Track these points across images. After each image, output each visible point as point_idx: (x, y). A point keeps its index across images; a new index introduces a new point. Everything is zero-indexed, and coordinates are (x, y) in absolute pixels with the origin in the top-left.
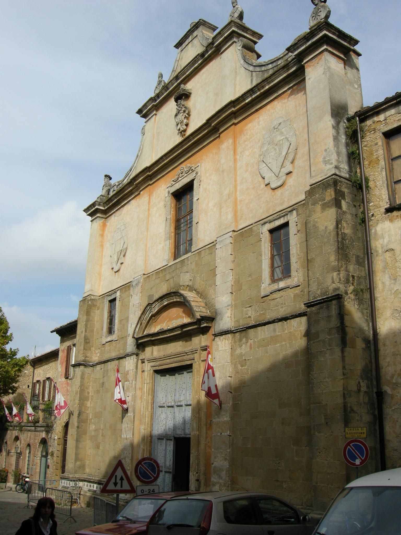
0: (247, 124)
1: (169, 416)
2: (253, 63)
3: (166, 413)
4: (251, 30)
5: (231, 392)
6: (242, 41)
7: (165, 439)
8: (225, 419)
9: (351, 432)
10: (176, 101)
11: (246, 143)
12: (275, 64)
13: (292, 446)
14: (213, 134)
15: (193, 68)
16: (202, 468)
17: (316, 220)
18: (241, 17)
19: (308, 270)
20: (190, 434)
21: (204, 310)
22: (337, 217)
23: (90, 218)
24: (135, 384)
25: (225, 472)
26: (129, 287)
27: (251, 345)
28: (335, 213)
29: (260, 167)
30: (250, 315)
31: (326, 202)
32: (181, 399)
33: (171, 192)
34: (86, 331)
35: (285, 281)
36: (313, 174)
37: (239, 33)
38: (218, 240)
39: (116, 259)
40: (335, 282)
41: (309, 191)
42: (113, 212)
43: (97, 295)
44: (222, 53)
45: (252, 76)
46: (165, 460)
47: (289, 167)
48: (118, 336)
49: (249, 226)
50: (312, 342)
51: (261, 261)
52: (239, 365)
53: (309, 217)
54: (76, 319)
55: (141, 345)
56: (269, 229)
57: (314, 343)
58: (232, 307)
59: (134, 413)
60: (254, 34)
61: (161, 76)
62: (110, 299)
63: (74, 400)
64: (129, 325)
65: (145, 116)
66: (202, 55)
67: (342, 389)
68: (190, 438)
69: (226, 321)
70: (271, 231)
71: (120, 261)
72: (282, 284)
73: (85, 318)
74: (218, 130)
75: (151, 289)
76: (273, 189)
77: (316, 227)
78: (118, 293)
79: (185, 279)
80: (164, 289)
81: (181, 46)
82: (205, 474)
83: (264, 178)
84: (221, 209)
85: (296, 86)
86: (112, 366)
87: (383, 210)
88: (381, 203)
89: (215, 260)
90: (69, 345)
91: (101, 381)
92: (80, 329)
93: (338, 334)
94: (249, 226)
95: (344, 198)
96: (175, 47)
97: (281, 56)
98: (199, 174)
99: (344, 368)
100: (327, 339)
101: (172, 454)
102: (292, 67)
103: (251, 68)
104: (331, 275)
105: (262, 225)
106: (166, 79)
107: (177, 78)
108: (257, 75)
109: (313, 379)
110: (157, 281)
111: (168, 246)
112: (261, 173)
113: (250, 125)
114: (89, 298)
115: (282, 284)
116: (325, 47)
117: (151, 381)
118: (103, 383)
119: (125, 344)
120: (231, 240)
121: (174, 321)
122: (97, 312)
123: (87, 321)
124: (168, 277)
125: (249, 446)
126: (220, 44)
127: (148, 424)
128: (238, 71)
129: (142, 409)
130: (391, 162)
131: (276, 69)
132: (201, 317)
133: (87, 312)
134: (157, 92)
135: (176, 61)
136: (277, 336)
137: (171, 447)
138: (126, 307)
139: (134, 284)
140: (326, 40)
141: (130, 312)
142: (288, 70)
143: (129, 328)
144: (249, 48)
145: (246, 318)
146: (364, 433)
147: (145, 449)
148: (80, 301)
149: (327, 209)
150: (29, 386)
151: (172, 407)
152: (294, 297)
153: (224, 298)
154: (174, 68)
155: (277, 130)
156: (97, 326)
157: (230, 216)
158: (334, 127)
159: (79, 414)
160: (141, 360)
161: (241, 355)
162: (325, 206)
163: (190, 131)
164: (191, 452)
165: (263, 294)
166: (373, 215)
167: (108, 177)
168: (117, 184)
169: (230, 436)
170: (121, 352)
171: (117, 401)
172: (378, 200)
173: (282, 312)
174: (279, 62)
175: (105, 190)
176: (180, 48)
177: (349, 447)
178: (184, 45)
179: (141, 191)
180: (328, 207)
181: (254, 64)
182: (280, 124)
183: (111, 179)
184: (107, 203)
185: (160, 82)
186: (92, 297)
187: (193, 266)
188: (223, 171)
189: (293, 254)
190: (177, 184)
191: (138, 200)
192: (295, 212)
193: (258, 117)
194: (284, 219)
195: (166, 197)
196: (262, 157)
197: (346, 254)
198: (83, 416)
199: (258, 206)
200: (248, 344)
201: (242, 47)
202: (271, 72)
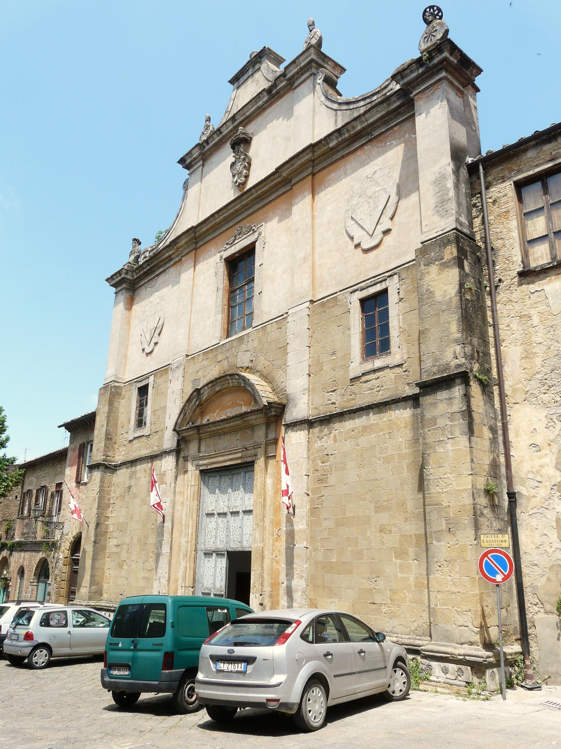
0: (329, 174)
1: (220, 525)
2: (338, 100)
3: (216, 522)
4: (333, 61)
5: (308, 495)
6: (322, 72)
7: (214, 554)
8: (300, 527)
9: (488, 539)
10: (233, 147)
11: (328, 196)
12: (368, 100)
13: (394, 559)
14: (282, 187)
15: (256, 107)
16: (267, 589)
17: (430, 283)
18: (319, 43)
19: (419, 343)
20: (251, 547)
21: (271, 395)
22: (460, 280)
23: (114, 290)
24: (175, 487)
25: (300, 593)
26: (167, 370)
27: (335, 436)
28: (458, 274)
29: (348, 225)
30: (333, 401)
31: (446, 261)
32: (237, 504)
33: (224, 257)
34: (107, 425)
35: (382, 359)
36: (424, 229)
37: (316, 65)
38: (290, 312)
39: (148, 338)
40: (458, 358)
41: (421, 249)
42: (143, 282)
43: (121, 381)
44: (295, 88)
45: (336, 115)
46: (215, 581)
47: (386, 224)
48: (151, 430)
49: (332, 294)
50: (426, 430)
51: (349, 336)
52: (319, 462)
53: (421, 279)
54: (94, 411)
55: (182, 442)
56: (360, 297)
57: (429, 431)
58: (309, 392)
59: (173, 522)
60: (336, 65)
61: (209, 119)
62: (140, 386)
63: (91, 509)
64: (167, 416)
65: (188, 167)
66: (269, 91)
67: (471, 487)
68: (250, 552)
69: (300, 409)
70: (363, 301)
71: (154, 341)
72: (378, 363)
73: (106, 409)
74: (291, 181)
75: (197, 372)
76: (366, 251)
77: (431, 293)
78: (152, 379)
79: (243, 360)
80: (214, 372)
81: (237, 81)
82: (271, 596)
83: (353, 238)
84: (293, 275)
85: (398, 126)
86: (140, 468)
87: (515, 273)
88: (510, 265)
89: (287, 336)
90: (81, 442)
91: (127, 485)
92: (100, 422)
93: (464, 420)
94: (332, 294)
95: (467, 259)
96: (229, 82)
97: (377, 90)
98: (263, 235)
99: (472, 461)
100: (448, 426)
101: (224, 572)
102: (395, 102)
103: (335, 106)
104: (453, 349)
105: (351, 293)
106: (215, 124)
107: (233, 119)
108: (343, 115)
109: (427, 475)
110: (206, 363)
111: (220, 321)
112: (349, 232)
113: (333, 175)
114: (113, 384)
115: (378, 363)
116: (444, 74)
117: (197, 483)
118: (130, 487)
119: (161, 438)
120: (307, 312)
121: (229, 410)
122: (123, 402)
123: (110, 412)
124: (220, 358)
125: (334, 560)
126: (293, 76)
127: (192, 535)
128: (317, 110)
129: (184, 518)
130: (523, 217)
131: (369, 106)
132: (268, 403)
133: (110, 401)
134: (204, 138)
135: (230, 99)
136: (372, 425)
137: (223, 563)
138: (163, 394)
139: (174, 367)
140: (444, 65)
141: (168, 400)
142: (389, 105)
143: (167, 420)
144: (331, 82)
145: (328, 404)
146: (505, 541)
147: (188, 567)
148: (101, 389)
149: (447, 269)
150: (16, 497)
151: (225, 514)
152: (395, 379)
153: (298, 381)
154: (227, 109)
155: (372, 179)
156: (122, 418)
157: (306, 283)
158: (454, 173)
159: (98, 525)
160: (183, 457)
161: (322, 448)
162: (445, 265)
163: (250, 185)
164: (252, 569)
165: (352, 376)
166: (500, 281)
167: (137, 241)
168: (150, 249)
169: (307, 548)
170: (155, 448)
171: (156, 506)
172: (507, 262)
173: (379, 397)
174: (375, 98)
175: (133, 257)
176: (236, 84)
177: (486, 558)
178: (242, 80)
179: (182, 257)
180: (448, 267)
181: (339, 101)
182: (375, 173)
183: (140, 243)
184: (137, 271)
185: (207, 127)
186: (116, 384)
187: (256, 343)
188: (296, 231)
189: (393, 327)
190: (233, 247)
191: (178, 267)
192: (396, 277)
193: (345, 165)
194: (381, 285)
195: (217, 263)
196: (350, 212)
197: (470, 325)
198: (102, 528)
199: (346, 270)
200: (332, 435)
201: (323, 81)
202: (362, 110)
